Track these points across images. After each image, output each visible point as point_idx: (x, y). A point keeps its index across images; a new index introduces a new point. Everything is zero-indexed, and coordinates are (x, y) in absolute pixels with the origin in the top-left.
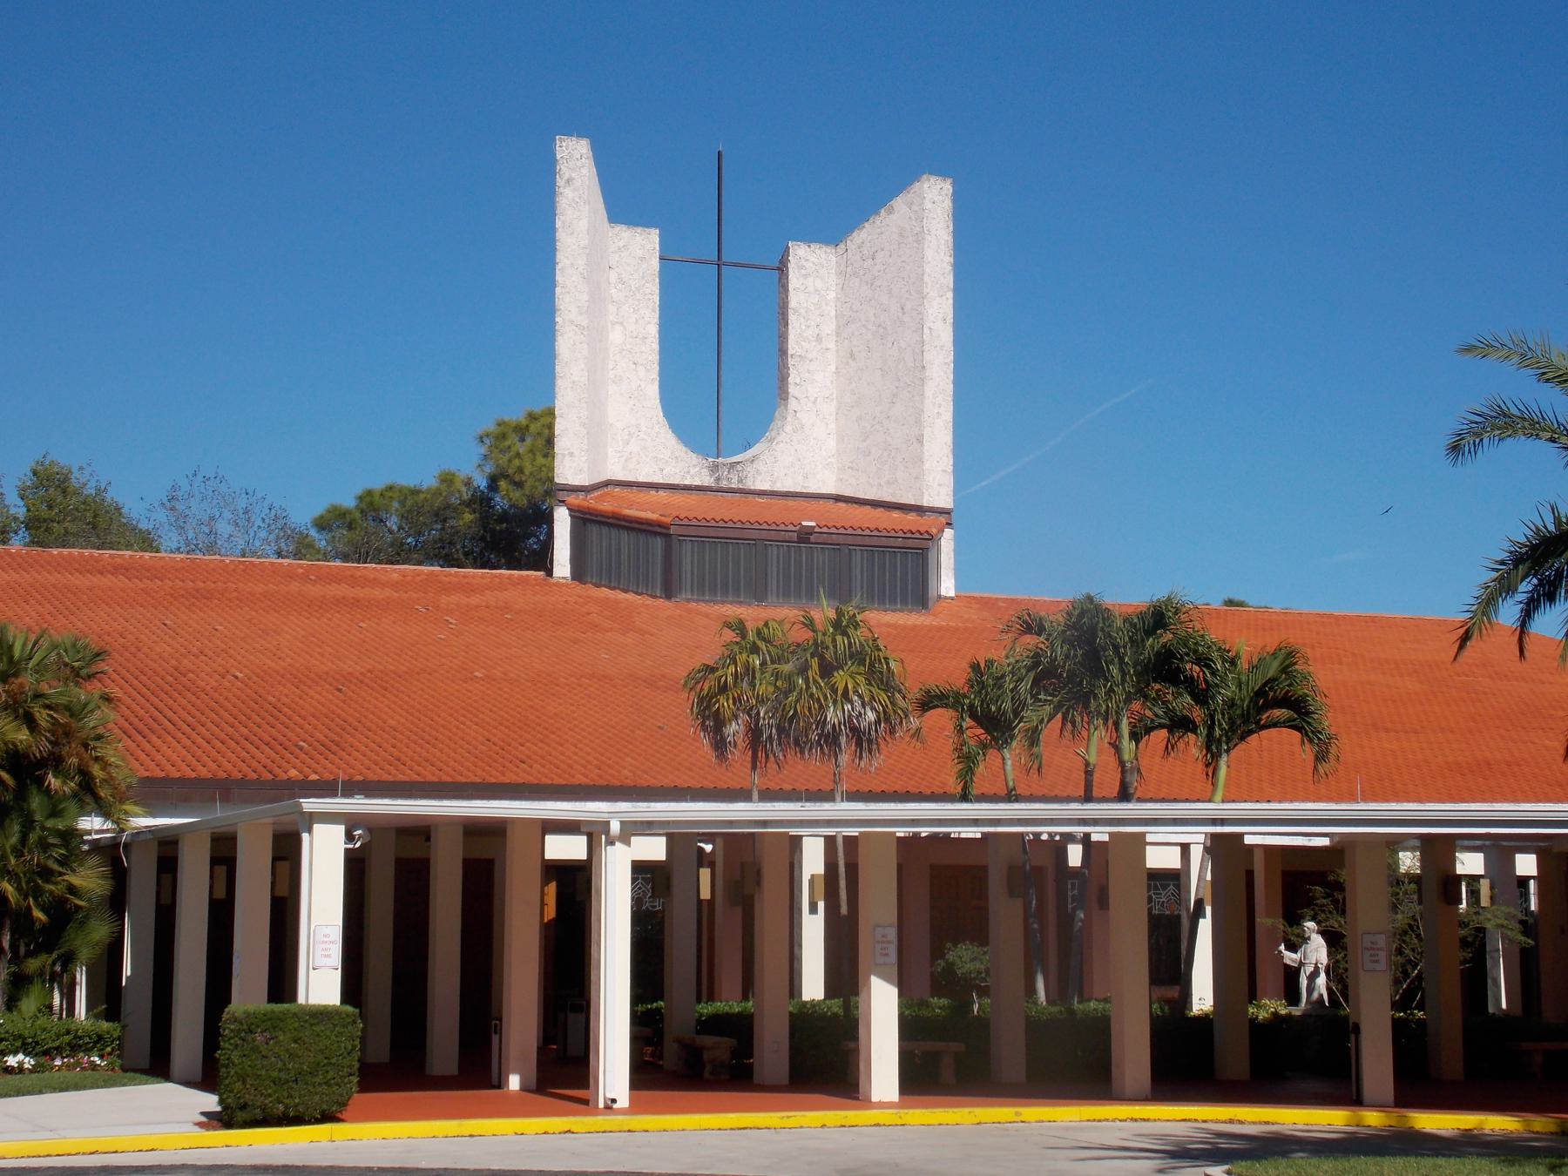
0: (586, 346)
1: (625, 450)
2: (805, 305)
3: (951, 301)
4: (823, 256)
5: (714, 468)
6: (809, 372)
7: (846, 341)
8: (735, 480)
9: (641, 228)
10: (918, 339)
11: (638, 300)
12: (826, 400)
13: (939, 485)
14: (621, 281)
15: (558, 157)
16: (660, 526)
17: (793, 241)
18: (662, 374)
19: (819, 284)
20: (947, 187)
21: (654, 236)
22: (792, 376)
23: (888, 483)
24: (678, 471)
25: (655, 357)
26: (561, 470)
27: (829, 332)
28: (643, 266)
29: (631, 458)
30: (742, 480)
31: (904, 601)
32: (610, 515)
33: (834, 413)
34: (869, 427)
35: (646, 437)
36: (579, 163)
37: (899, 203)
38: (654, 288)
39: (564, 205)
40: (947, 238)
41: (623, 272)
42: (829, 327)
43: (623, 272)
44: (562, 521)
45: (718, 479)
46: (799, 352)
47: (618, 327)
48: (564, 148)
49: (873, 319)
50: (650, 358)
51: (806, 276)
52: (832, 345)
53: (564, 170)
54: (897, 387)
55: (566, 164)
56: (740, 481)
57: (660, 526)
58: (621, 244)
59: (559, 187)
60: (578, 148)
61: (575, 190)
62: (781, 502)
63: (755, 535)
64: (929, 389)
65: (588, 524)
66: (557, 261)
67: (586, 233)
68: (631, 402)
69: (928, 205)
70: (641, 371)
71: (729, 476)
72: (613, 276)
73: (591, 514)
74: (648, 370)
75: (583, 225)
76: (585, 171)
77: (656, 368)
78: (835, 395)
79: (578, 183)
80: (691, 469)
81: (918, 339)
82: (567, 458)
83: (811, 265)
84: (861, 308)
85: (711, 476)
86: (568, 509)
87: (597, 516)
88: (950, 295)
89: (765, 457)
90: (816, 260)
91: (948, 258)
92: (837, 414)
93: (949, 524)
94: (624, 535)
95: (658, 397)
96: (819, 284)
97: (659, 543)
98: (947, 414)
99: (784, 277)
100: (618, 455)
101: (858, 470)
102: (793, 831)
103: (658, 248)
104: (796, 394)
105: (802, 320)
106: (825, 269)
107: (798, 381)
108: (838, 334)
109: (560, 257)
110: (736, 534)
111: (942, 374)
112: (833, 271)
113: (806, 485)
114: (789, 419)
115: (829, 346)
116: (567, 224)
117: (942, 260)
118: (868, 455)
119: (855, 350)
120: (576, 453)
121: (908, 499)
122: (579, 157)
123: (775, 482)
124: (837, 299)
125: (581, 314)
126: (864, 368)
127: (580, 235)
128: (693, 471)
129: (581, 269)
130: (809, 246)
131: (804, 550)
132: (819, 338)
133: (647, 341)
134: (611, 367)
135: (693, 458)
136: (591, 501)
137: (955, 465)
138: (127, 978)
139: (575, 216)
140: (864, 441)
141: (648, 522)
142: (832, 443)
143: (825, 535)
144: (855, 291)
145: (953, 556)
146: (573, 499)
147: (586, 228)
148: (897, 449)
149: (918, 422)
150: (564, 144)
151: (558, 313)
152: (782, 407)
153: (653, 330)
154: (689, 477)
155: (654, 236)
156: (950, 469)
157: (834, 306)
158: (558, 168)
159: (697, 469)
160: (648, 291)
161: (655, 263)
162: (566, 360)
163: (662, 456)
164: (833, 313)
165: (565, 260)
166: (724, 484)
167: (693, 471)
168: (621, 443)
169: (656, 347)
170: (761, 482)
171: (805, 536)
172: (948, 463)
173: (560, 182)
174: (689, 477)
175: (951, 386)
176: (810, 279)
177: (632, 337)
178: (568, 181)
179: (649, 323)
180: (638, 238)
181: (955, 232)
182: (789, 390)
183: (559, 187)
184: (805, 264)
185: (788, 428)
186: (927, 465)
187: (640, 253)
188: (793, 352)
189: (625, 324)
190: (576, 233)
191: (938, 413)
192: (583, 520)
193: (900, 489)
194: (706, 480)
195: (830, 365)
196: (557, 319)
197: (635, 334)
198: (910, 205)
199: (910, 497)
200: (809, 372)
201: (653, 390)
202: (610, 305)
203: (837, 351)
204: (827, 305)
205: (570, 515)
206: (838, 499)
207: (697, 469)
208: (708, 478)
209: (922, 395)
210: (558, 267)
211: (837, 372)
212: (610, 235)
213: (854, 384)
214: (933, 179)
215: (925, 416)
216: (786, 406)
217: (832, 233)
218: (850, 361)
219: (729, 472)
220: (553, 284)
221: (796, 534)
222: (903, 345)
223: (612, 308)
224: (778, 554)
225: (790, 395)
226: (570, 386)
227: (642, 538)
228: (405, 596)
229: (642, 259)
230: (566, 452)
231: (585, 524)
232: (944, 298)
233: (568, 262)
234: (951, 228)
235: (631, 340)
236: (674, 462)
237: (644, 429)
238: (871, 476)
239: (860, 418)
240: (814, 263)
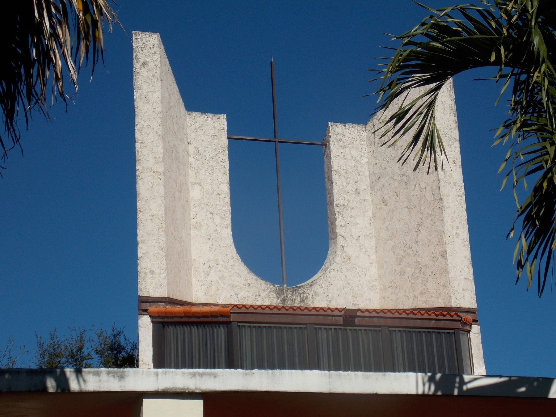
0: (162, 187)
1: (206, 279)
2: (345, 168)
3: (458, 149)
4: (356, 132)
5: (280, 292)
6: (351, 216)
7: (379, 192)
8: (298, 300)
9: (212, 114)
10: (435, 178)
11: (212, 166)
12: (367, 238)
13: (463, 290)
14: (198, 152)
15: (135, 46)
16: (222, 316)
17: (331, 122)
18: (233, 220)
19: (354, 153)
21: (223, 119)
22: (338, 220)
23: (422, 294)
24: (250, 295)
25: (228, 208)
26: (143, 286)
27: (365, 187)
28: (215, 141)
29: (211, 286)
30: (303, 300)
32: (183, 315)
33: (374, 247)
34: (403, 253)
35: (223, 269)
36: (152, 51)
38: (224, 158)
39: (141, 82)
40: (451, 103)
41: (199, 146)
42: (365, 184)
43: (199, 146)
45: (284, 300)
46: (343, 202)
47: (197, 187)
48: (139, 40)
49: (398, 171)
50: (224, 209)
51: (343, 147)
52: (368, 197)
54: (421, 218)
55: (141, 52)
56: (302, 301)
57: (222, 316)
58: (197, 125)
59: (136, 69)
60: (151, 40)
61: (149, 71)
63: (305, 320)
64: (447, 215)
65: (166, 327)
66: (136, 122)
67: (159, 102)
68: (210, 243)
70: (217, 219)
71: (293, 297)
72: (191, 149)
73: (167, 317)
74: (222, 218)
75: (157, 96)
76: (157, 57)
77: (229, 216)
78: (373, 234)
79: (151, 65)
80: (261, 293)
81: (435, 178)
82: (149, 275)
83: (348, 139)
84: (388, 165)
85: (278, 298)
86: (150, 316)
87: (172, 318)
88: (457, 144)
89: (321, 282)
90: (351, 136)
91: (453, 117)
92: (376, 247)
93: (475, 321)
94: (195, 329)
95: (231, 238)
96: (354, 153)
97: (222, 331)
98: (464, 233)
99: (327, 149)
100: (201, 283)
101: (396, 288)
103: (226, 129)
104: (343, 234)
105: (343, 178)
106: (358, 141)
107: (343, 224)
108: (372, 188)
109: (138, 120)
110: (290, 319)
111: (457, 203)
112: (365, 143)
113: (355, 303)
114: (338, 252)
115: (365, 198)
116: (143, 96)
117: (448, 119)
118: (404, 275)
119: (386, 197)
120: (157, 271)
122: (151, 46)
123: (330, 301)
124: (370, 163)
125: (157, 163)
126: (395, 209)
127: (155, 104)
128: (263, 294)
129: (156, 129)
130: (345, 126)
131: (349, 332)
132: (357, 192)
133: (221, 196)
134: (192, 216)
135: (262, 284)
137: (475, 274)
139: (150, 90)
140: (399, 264)
142: (374, 271)
143: (367, 319)
144: (383, 154)
145: (481, 347)
146: (153, 308)
147: (160, 98)
148: (426, 266)
149: (441, 242)
150: (139, 37)
151: (137, 163)
152: (333, 245)
153: (225, 188)
154: (259, 299)
155: (223, 119)
156: (471, 277)
157: (367, 168)
158: (135, 54)
159: (266, 293)
160: (220, 160)
161: (224, 140)
162: (145, 198)
163: (237, 284)
164: (367, 173)
165: (143, 122)
167: (263, 294)
168: (202, 274)
169: (228, 200)
170: (320, 302)
172: (469, 272)
174: (259, 299)
175: (465, 213)
176: (347, 149)
177: (208, 193)
178: (144, 64)
179: (222, 183)
180: (210, 122)
182: (337, 231)
183: (136, 69)
184: (342, 138)
185: (338, 259)
186: (452, 274)
187: (212, 132)
188: (338, 202)
189: (202, 185)
190: (151, 102)
191: (457, 233)
193: (432, 297)
195: (367, 211)
196: (137, 167)
197: (211, 191)
199: (440, 301)
200: (351, 216)
201: (227, 233)
202: (190, 171)
203: (372, 201)
204: (362, 167)
205: (152, 322)
207: (266, 293)
208: (276, 299)
209: (442, 220)
210: (137, 128)
211: (374, 216)
212: (188, 119)
213: (387, 223)
215: (447, 236)
216: (335, 242)
218: (383, 206)
219: (292, 295)
220: (132, 140)
221: (341, 318)
222: (423, 185)
223: (191, 173)
224: (328, 338)
225: (338, 234)
226: (150, 218)
229: (214, 136)
230: (148, 271)
231: (164, 327)
232: (453, 146)
233: (145, 124)
234: (453, 96)
235: (208, 196)
236: (247, 287)
237: (221, 263)
238: (407, 290)
239: (394, 247)
240: (349, 137)
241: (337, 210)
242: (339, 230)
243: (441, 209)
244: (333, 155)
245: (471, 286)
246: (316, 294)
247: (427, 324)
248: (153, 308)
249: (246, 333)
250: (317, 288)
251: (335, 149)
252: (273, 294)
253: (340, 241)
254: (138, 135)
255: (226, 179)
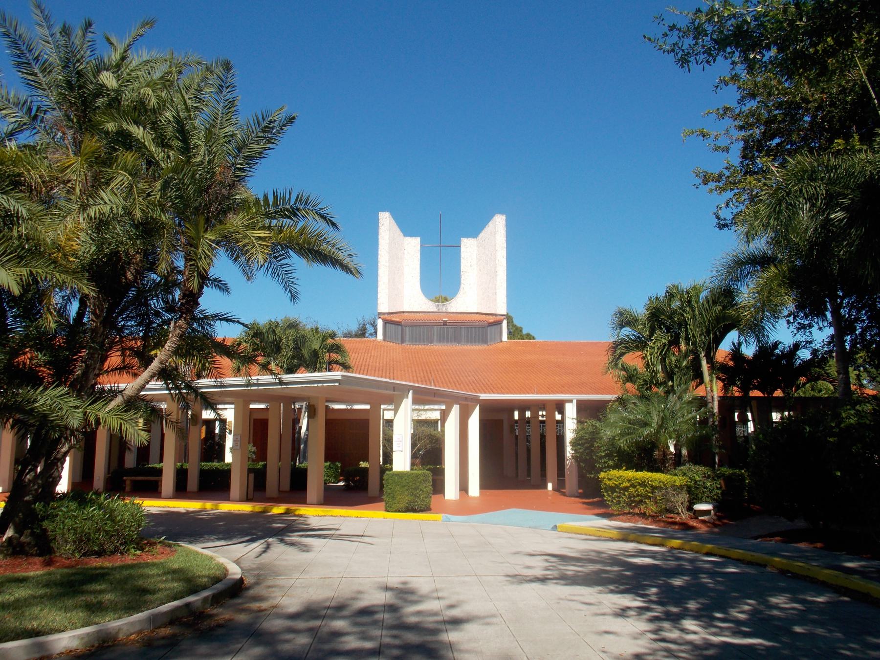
20: (504, 217)
21: (418, 239)
31: (479, 342)
37: (490, 224)
44: (380, 324)
45: (439, 309)
53: (381, 221)
62: (459, 315)
69: (497, 223)
79: (385, 225)
88: (505, 249)
97: (400, 327)
98: (505, 285)
102: (252, 421)
109: (380, 247)
121: (493, 312)
132: (471, 266)
135: (431, 303)
136: (386, 317)
138: (574, 444)
141: (397, 322)
146: (383, 316)
149: (495, 288)
153: (418, 267)
155: (418, 239)
156: (505, 302)
161: (419, 247)
166: (441, 311)
169: (419, 271)
171: (445, 323)
172: (505, 300)
173: (380, 225)
181: (506, 231)
192: (386, 322)
194: (435, 310)
198: (493, 224)
201: (418, 284)
206: (477, 313)
214: (499, 215)
217: (474, 234)
220: (377, 254)
227: (397, 326)
228: (472, 348)
241: (462, 273)
242: (462, 282)
243: (496, 276)
244: (462, 251)
245: (505, 306)
246: (452, 307)
247: (474, 324)
248: (383, 316)
249: (408, 328)
250: (452, 304)
251: (463, 249)
252: (435, 307)
253: (462, 286)
254: (379, 252)
255: (419, 263)
